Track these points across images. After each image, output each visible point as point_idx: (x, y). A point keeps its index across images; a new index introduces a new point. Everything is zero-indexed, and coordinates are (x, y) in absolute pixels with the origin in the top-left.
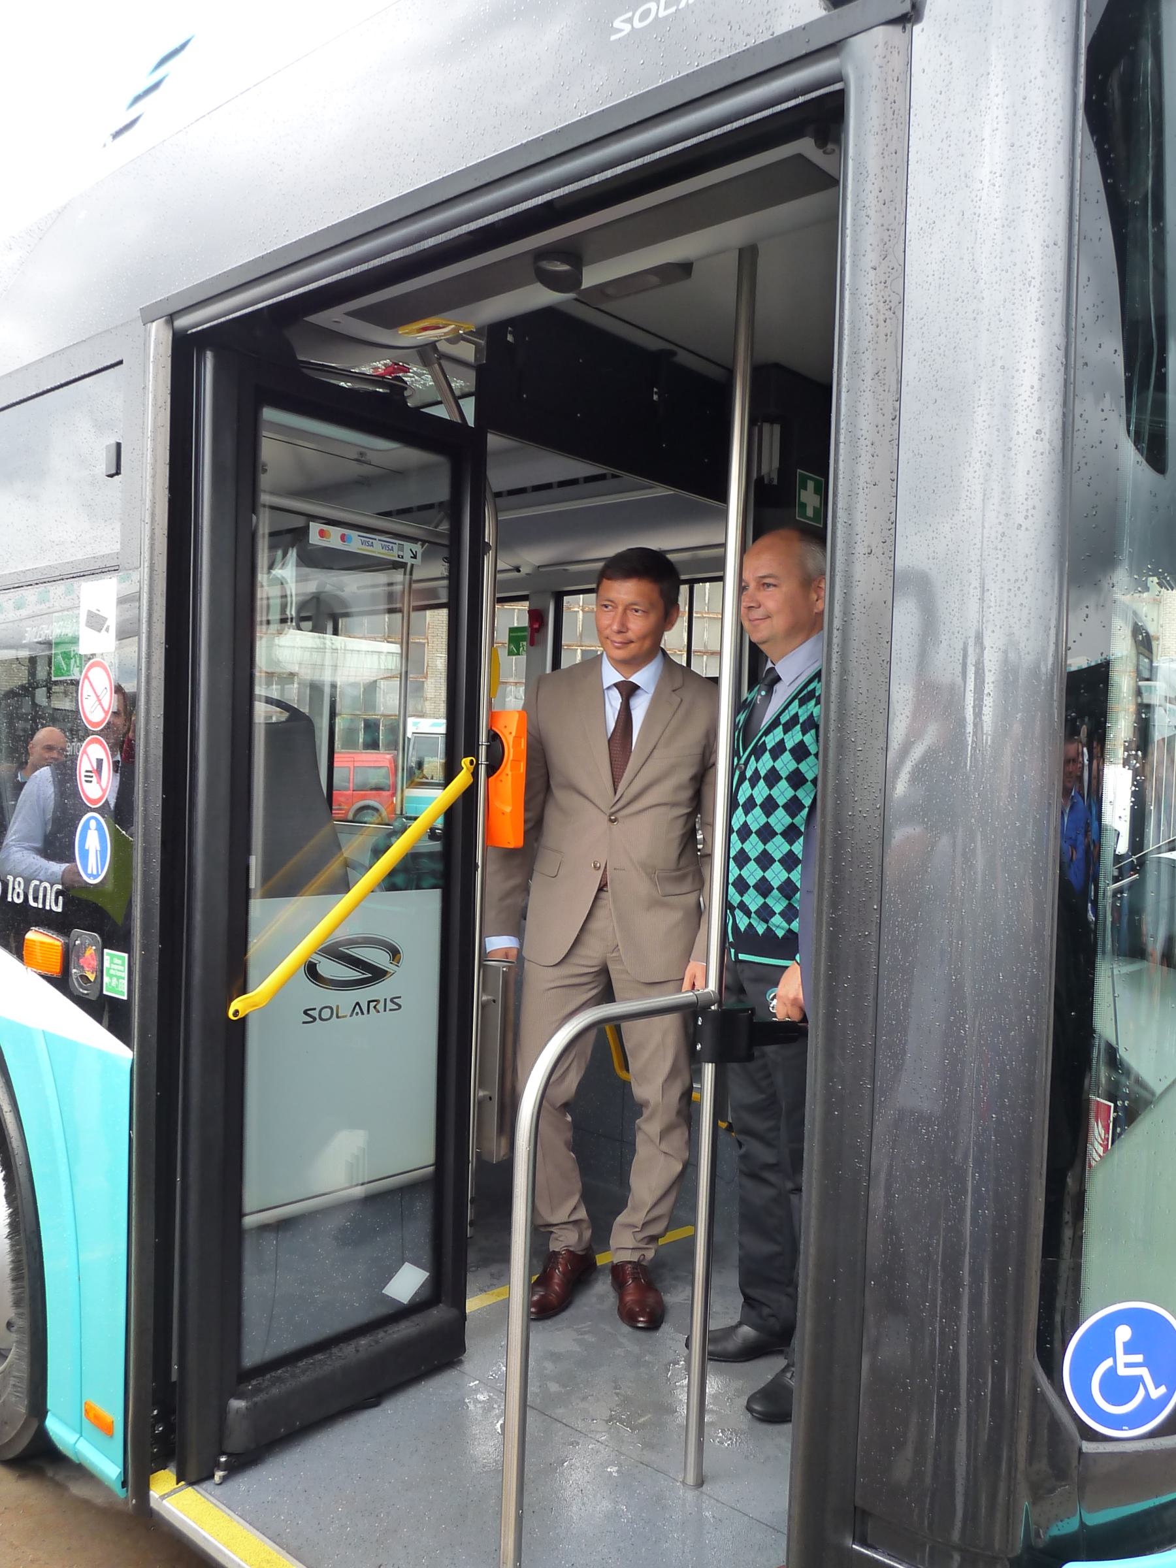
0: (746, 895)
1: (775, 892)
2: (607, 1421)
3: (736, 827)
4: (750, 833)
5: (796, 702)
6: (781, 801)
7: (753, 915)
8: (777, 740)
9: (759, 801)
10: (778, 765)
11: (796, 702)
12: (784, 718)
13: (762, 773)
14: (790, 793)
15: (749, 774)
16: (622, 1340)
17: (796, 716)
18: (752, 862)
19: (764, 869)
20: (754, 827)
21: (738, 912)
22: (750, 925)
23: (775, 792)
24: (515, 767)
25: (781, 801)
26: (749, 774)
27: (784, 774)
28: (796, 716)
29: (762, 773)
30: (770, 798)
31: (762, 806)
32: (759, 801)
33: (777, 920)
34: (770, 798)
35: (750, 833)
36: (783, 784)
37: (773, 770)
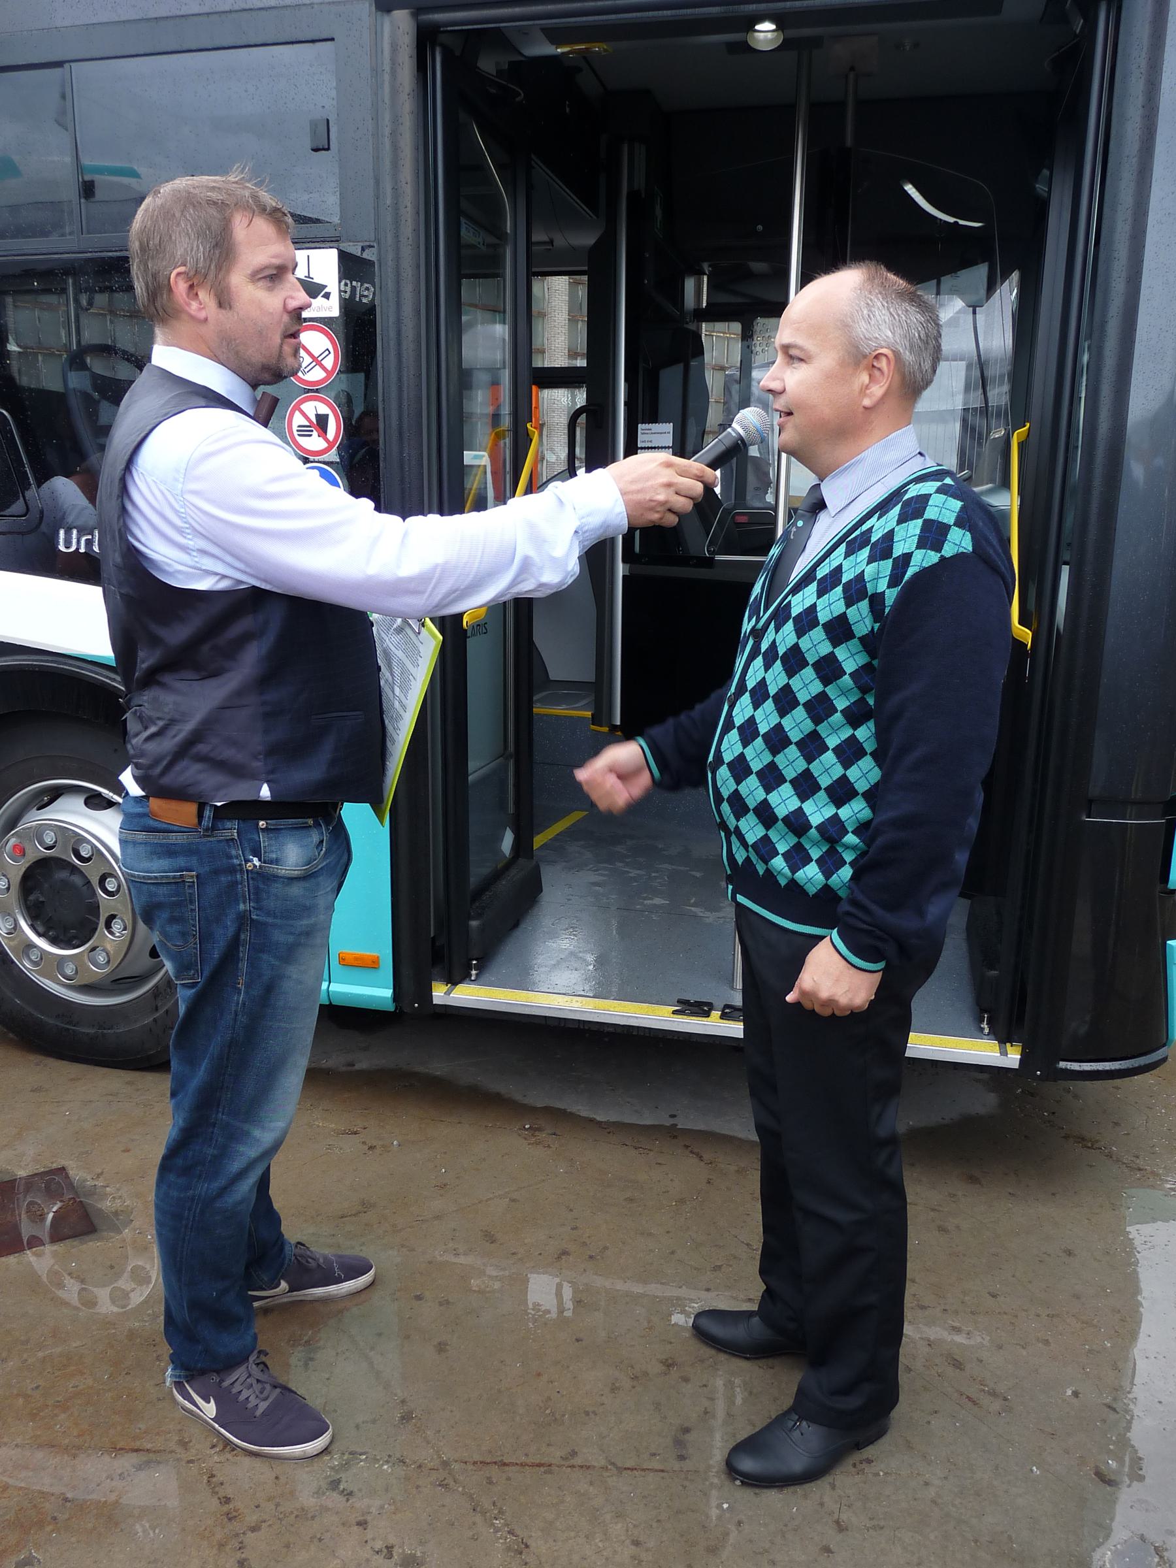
0: (743, 820)
1: (780, 824)
2: (441, 1304)
3: (751, 684)
4: (814, 623)
5: (842, 548)
6: (803, 697)
7: (750, 849)
8: (808, 604)
9: (772, 690)
10: (805, 644)
11: (842, 548)
12: (821, 572)
13: (781, 650)
14: (817, 687)
15: (764, 646)
16: (226, 1384)
17: (839, 569)
18: (802, 701)
19: (768, 789)
20: (823, 616)
21: (734, 838)
22: (748, 859)
23: (796, 683)
24: (402, 742)
25: (803, 697)
26: (764, 646)
27: (811, 658)
28: (839, 569)
29: (781, 650)
30: (787, 689)
31: (777, 698)
32: (772, 690)
33: (778, 863)
34: (787, 689)
35: (814, 623)
36: (808, 673)
37: (795, 650)
